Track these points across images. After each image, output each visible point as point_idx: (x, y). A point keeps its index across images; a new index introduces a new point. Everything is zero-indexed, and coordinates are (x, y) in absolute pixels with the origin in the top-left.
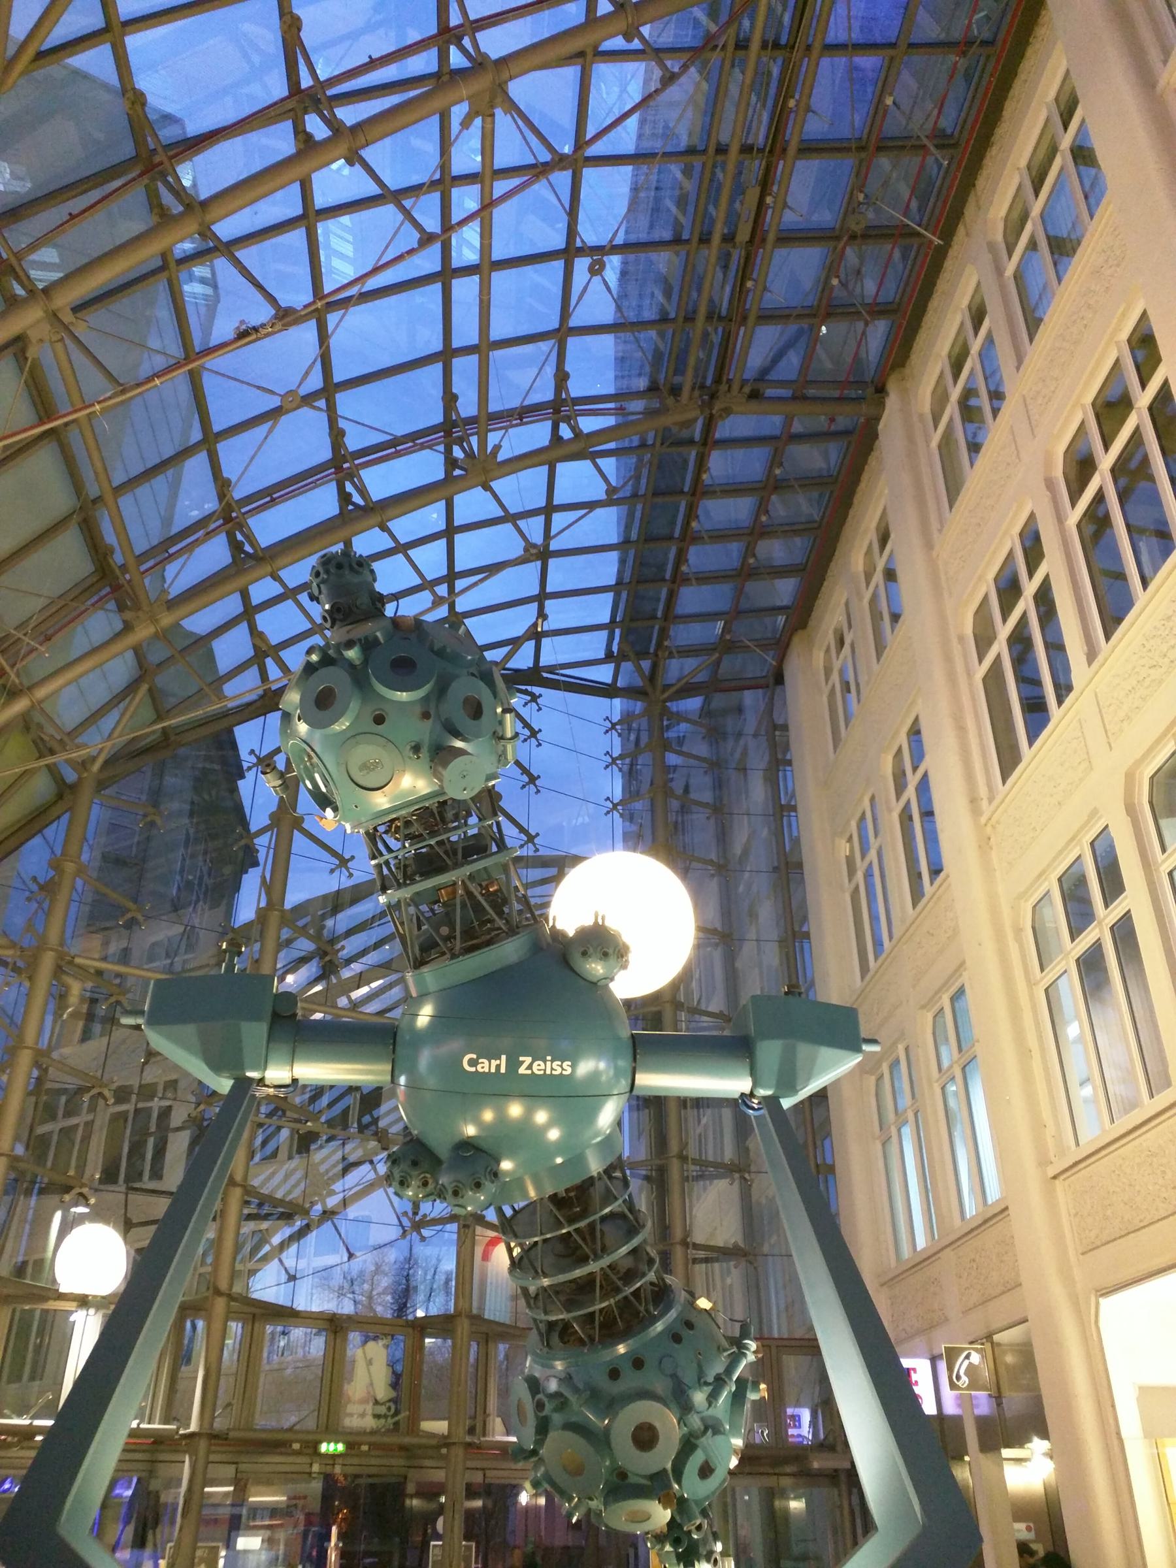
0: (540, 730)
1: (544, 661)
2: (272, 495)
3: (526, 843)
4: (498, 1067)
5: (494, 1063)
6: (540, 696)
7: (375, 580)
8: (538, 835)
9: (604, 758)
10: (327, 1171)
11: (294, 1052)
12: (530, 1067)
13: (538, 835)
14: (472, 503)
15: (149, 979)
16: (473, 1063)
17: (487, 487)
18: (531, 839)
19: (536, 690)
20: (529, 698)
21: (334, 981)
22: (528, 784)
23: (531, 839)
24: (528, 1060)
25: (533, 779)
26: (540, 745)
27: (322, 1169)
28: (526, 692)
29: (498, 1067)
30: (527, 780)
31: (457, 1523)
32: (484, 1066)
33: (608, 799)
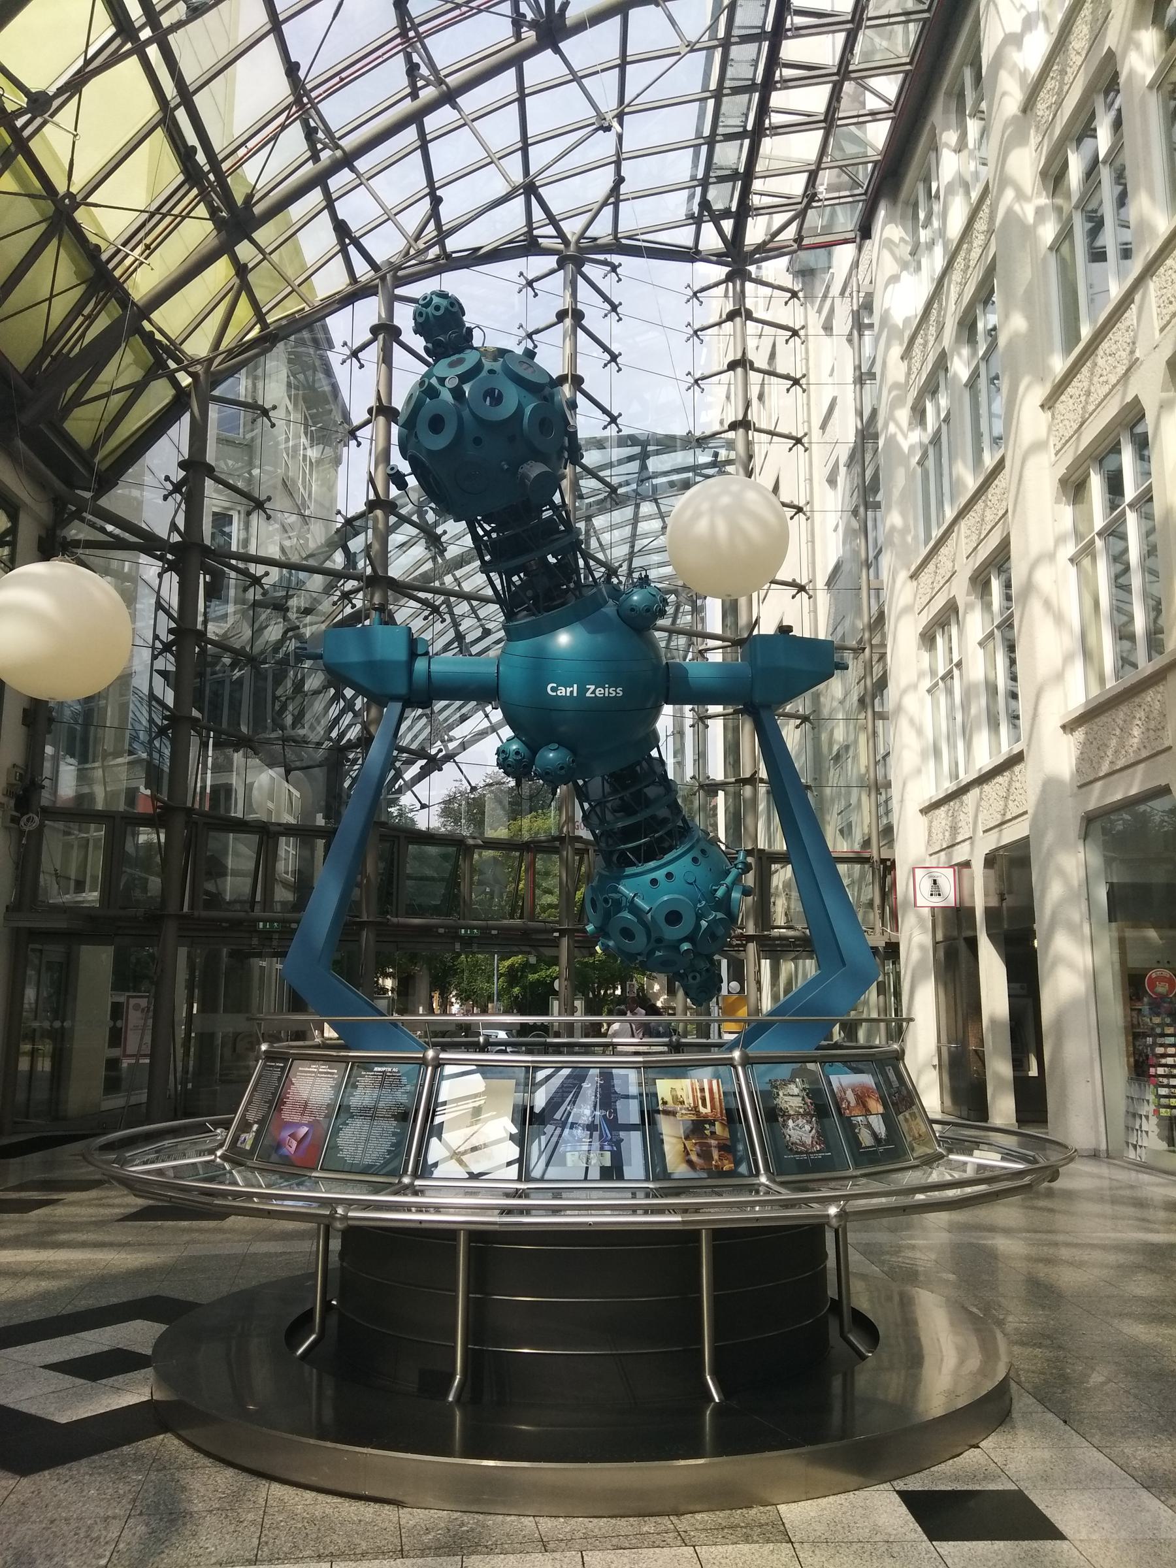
0: (620, 304)
1: (624, 226)
2: (341, 78)
3: (609, 424)
4: (572, 692)
5: (569, 690)
6: (620, 265)
7: (464, 314)
8: (620, 415)
9: (685, 329)
10: (446, 720)
11: (429, 676)
12: (594, 692)
13: (620, 415)
14: (542, 67)
15: (560, 1014)
16: (554, 689)
17: (557, 51)
18: (613, 420)
19: (615, 259)
20: (609, 268)
21: (440, 561)
22: (609, 362)
23: (613, 420)
24: (593, 687)
25: (614, 358)
26: (620, 319)
27: (441, 718)
28: (605, 263)
29: (572, 692)
30: (608, 358)
31: (883, 1200)
32: (562, 692)
33: (689, 373)
